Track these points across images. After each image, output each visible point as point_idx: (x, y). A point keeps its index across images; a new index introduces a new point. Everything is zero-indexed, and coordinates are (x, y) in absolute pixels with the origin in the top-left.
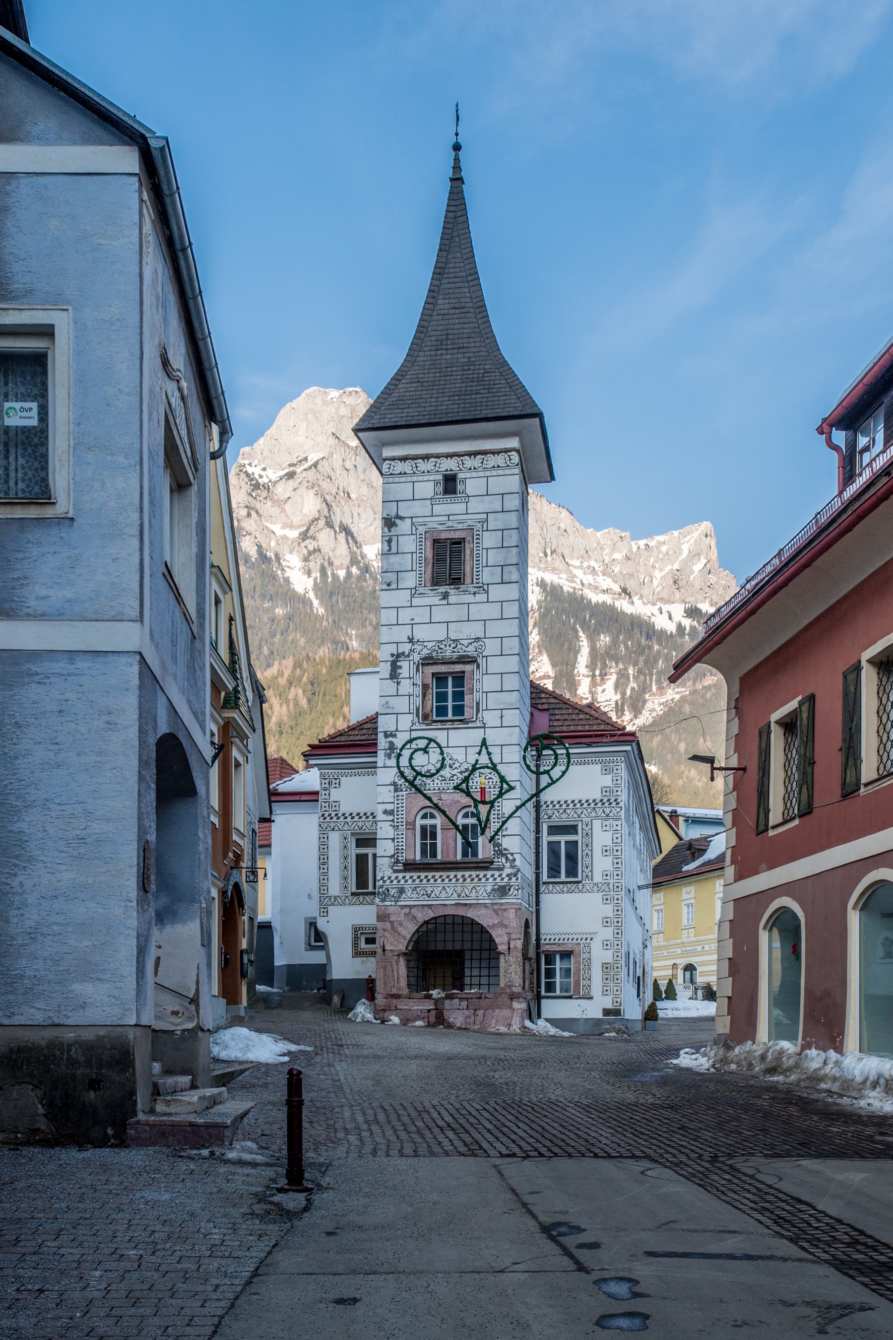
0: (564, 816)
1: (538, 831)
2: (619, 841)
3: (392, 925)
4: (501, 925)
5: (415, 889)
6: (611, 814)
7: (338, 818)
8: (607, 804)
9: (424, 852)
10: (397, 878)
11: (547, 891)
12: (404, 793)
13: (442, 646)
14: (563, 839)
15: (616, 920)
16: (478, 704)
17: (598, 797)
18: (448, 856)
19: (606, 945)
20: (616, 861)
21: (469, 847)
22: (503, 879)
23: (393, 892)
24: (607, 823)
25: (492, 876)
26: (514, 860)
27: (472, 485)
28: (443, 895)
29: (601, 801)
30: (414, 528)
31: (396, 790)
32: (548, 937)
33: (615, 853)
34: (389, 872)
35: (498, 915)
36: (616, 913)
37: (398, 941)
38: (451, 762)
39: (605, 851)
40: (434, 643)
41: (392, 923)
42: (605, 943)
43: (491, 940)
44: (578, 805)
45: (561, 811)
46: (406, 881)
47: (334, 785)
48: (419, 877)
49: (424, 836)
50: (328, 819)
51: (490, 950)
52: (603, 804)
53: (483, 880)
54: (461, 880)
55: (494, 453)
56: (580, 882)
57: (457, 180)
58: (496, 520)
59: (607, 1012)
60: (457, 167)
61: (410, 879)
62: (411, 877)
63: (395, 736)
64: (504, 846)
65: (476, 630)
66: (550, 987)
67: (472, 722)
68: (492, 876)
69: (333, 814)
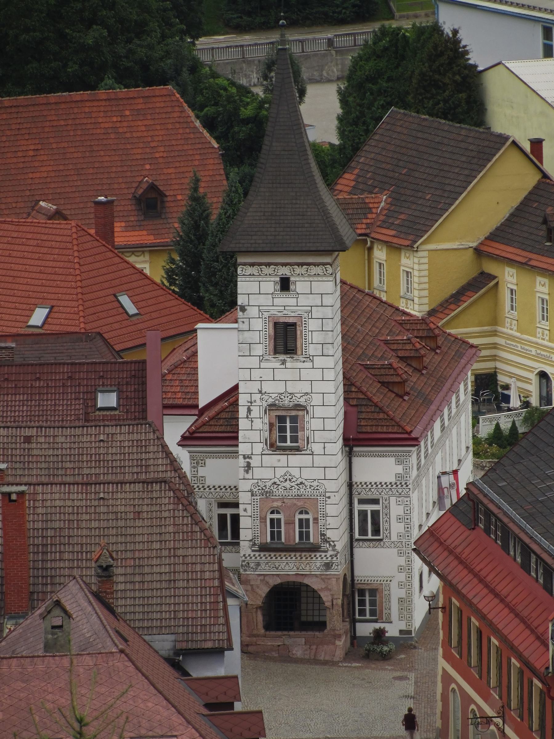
0: (370, 493)
1: (351, 503)
2: (408, 512)
3: (253, 589)
4: (327, 589)
5: (267, 563)
7: (205, 489)
9: (272, 538)
10: (254, 555)
13: (282, 397)
14: (369, 508)
15: (407, 568)
16: (308, 438)
17: (393, 480)
18: (289, 541)
19: (401, 585)
20: (406, 526)
21: (304, 535)
22: (327, 558)
23: (252, 565)
24: (400, 499)
25: (320, 556)
26: (335, 546)
27: (300, 286)
29: (396, 483)
31: (252, 495)
32: (360, 579)
33: (406, 521)
34: (249, 552)
35: (324, 582)
36: (407, 563)
38: (290, 477)
39: (399, 519)
40: (276, 395)
41: (252, 585)
43: (320, 597)
46: (261, 558)
47: (200, 465)
49: (272, 526)
50: (201, 486)
52: (397, 486)
53: (314, 558)
54: (299, 558)
55: (315, 265)
56: (381, 540)
58: (317, 311)
59: (401, 632)
61: (263, 557)
62: (264, 555)
63: (251, 458)
64: (328, 536)
66: (362, 612)
68: (320, 556)
69: (201, 486)
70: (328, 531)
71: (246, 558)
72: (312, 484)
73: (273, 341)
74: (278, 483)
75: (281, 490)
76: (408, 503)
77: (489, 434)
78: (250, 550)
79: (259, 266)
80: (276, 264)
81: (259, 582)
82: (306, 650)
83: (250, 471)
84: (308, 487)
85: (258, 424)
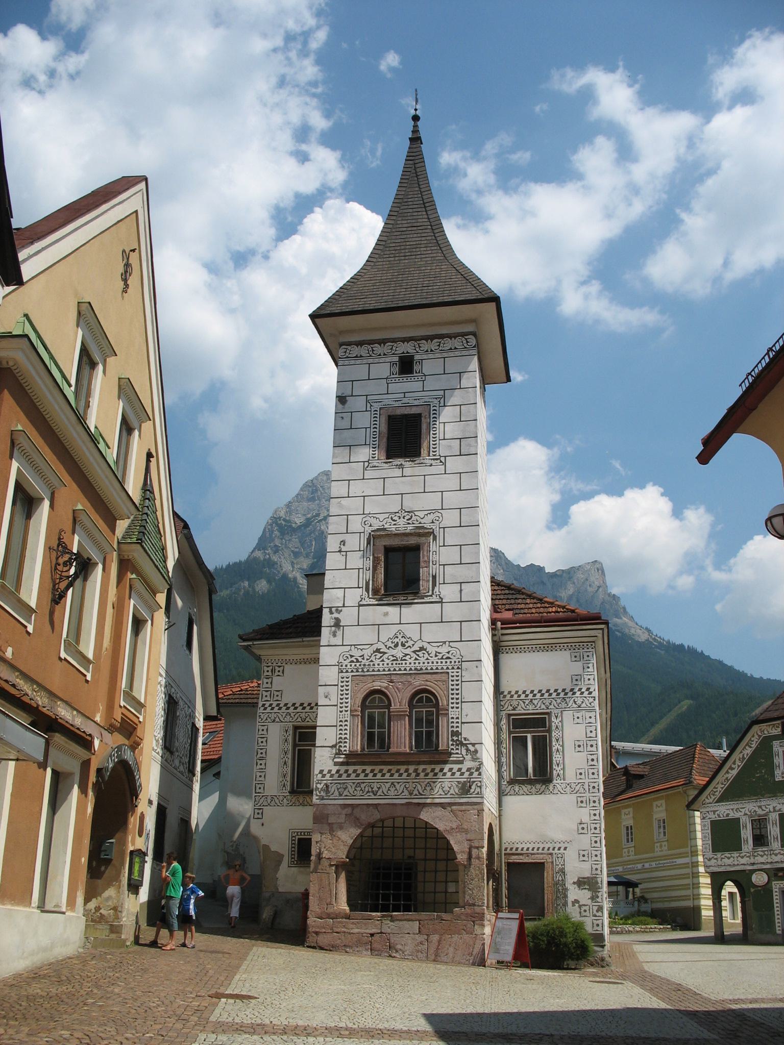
0: (531, 707)
4: (460, 829)
6: (584, 705)
7: (280, 709)
8: (578, 694)
11: (512, 792)
12: (350, 674)
16: (434, 577)
20: (590, 757)
22: (462, 774)
24: (579, 715)
26: (476, 751)
27: (430, 365)
28: (392, 792)
29: (572, 690)
30: (369, 405)
35: (456, 816)
37: (335, 846)
38: (404, 640)
42: (582, 853)
43: (449, 848)
44: (546, 695)
45: (527, 702)
47: (277, 673)
48: (364, 771)
51: (447, 860)
54: (414, 775)
55: (450, 336)
57: (416, 139)
60: (415, 131)
65: (432, 501)
67: (427, 596)
69: (275, 704)
70: (464, 726)
71: (324, 776)
72: (439, 650)
73: (385, 440)
74: (384, 649)
75: (387, 661)
76: (593, 720)
77: (767, 39)
78: (331, 763)
79: (369, 344)
80: (394, 340)
81: (342, 819)
82: (421, 943)
83: (339, 633)
84: (433, 654)
85: (356, 561)
